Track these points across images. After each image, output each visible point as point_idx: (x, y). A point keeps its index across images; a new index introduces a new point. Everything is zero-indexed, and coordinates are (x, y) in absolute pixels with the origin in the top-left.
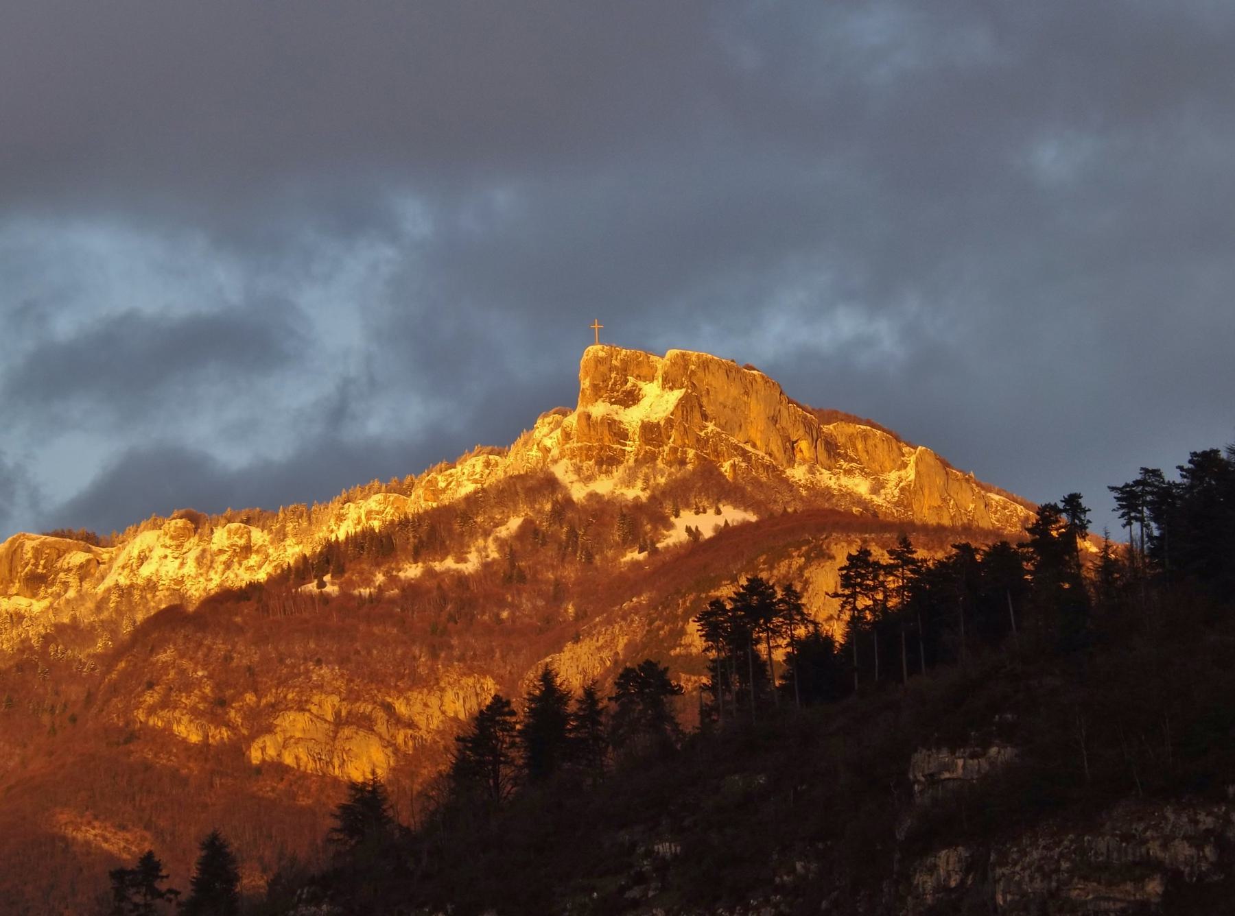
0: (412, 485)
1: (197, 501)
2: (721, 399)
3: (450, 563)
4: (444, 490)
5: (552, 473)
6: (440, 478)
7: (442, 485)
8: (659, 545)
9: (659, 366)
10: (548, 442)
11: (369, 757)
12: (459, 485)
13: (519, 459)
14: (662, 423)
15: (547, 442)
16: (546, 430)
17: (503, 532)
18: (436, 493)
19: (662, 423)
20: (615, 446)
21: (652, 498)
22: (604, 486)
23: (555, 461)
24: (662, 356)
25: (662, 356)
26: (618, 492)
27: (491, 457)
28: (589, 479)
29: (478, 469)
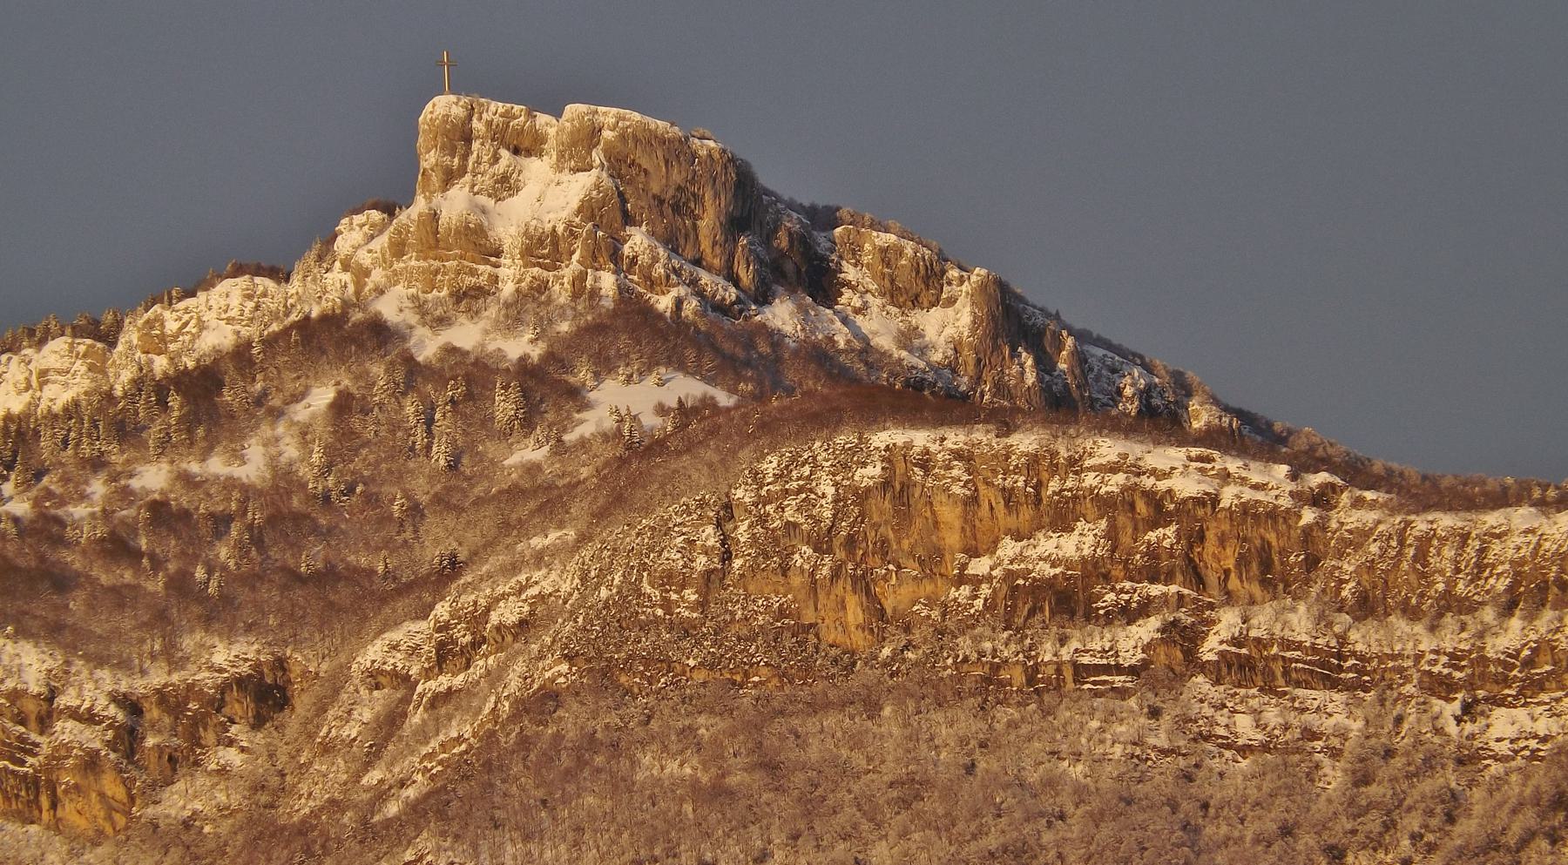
0: (118, 326)
1: (1305, 662)
2: (655, 188)
3: (217, 466)
4: (175, 337)
5: (378, 315)
6: (167, 314)
7: (172, 326)
8: (566, 438)
9: (552, 131)
10: (364, 258)
11: (102, 795)
12: (202, 326)
13: (317, 290)
14: (560, 229)
15: (361, 261)
16: (357, 236)
17: (300, 412)
18: (156, 342)
19: (560, 229)
20: (481, 268)
21: (549, 357)
22: (467, 335)
23: (380, 291)
24: (558, 114)
25: (558, 114)
26: (491, 347)
27: (258, 280)
28: (442, 322)
29: (235, 301)
